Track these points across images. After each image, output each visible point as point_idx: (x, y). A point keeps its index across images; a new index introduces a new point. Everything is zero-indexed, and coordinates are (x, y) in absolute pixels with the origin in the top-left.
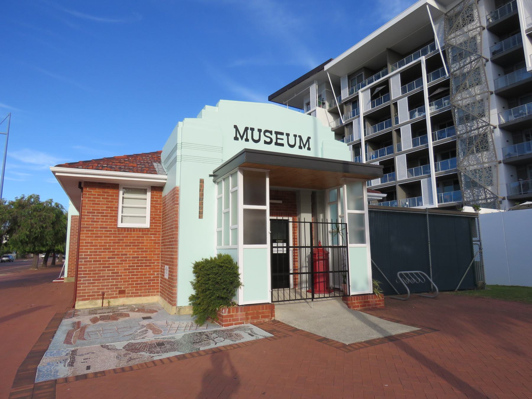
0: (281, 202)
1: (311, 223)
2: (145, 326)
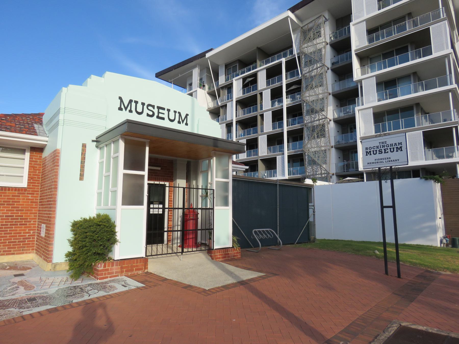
0: (159, 168)
1: (184, 188)
2: (16, 283)
